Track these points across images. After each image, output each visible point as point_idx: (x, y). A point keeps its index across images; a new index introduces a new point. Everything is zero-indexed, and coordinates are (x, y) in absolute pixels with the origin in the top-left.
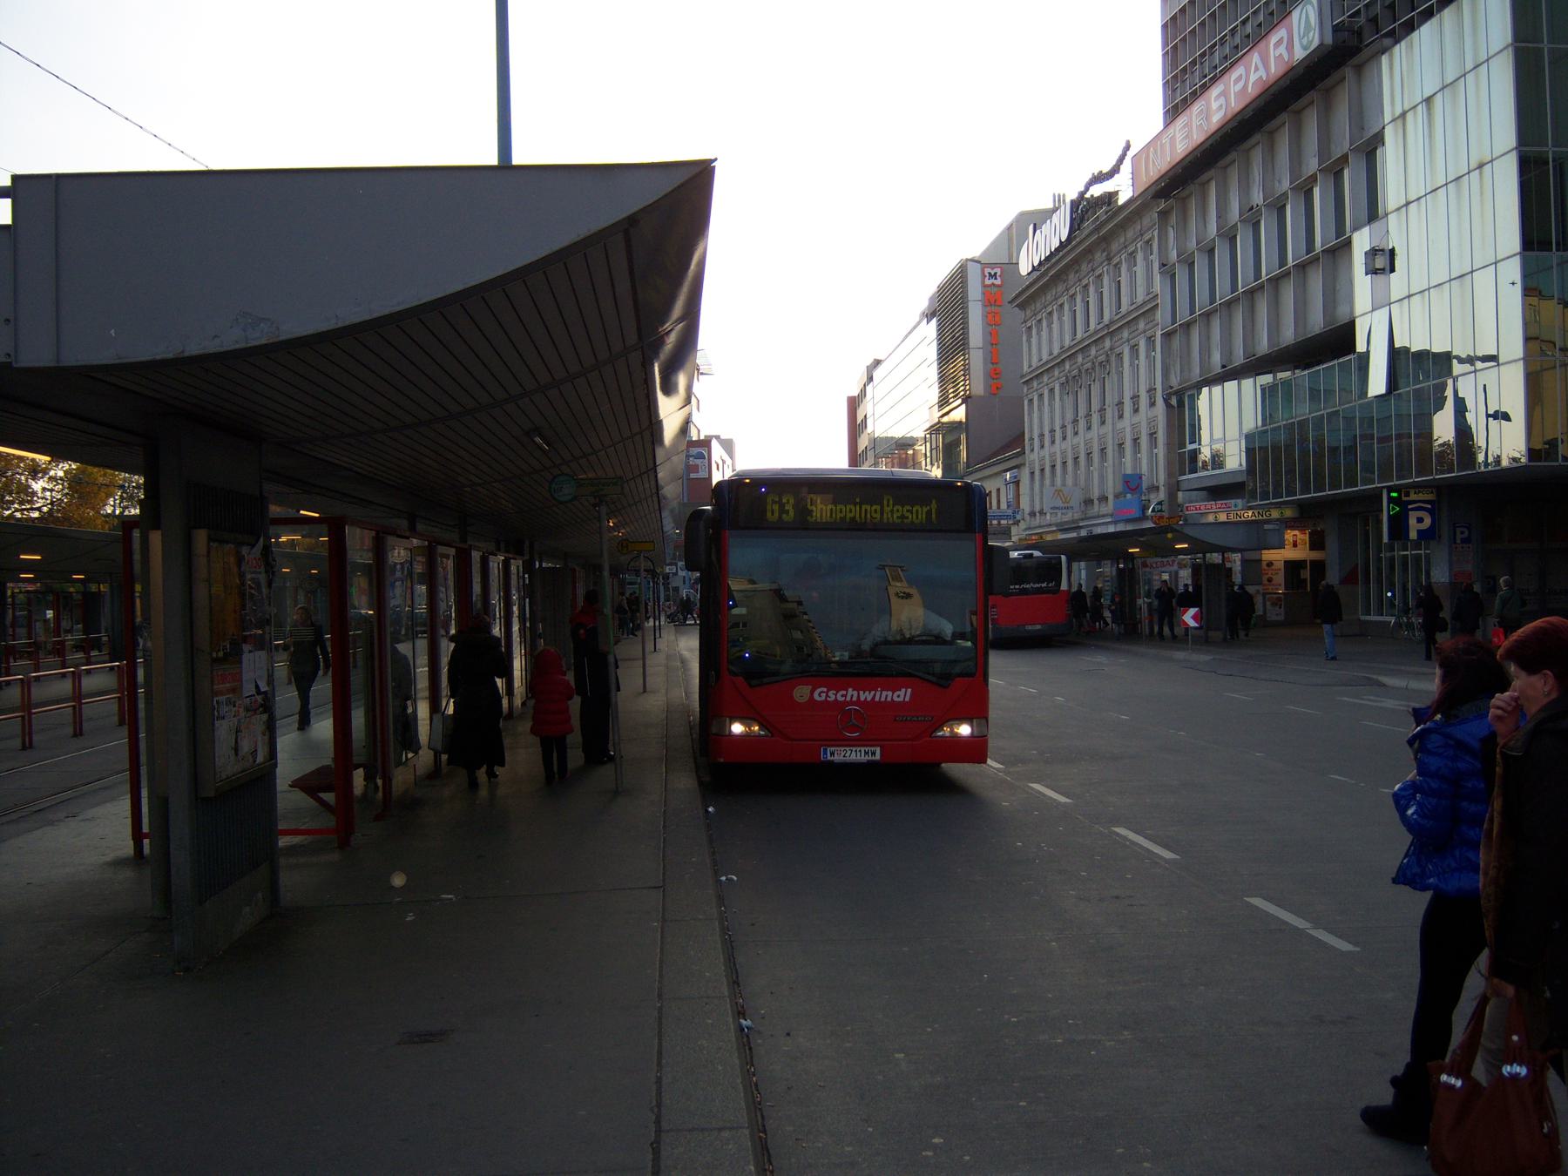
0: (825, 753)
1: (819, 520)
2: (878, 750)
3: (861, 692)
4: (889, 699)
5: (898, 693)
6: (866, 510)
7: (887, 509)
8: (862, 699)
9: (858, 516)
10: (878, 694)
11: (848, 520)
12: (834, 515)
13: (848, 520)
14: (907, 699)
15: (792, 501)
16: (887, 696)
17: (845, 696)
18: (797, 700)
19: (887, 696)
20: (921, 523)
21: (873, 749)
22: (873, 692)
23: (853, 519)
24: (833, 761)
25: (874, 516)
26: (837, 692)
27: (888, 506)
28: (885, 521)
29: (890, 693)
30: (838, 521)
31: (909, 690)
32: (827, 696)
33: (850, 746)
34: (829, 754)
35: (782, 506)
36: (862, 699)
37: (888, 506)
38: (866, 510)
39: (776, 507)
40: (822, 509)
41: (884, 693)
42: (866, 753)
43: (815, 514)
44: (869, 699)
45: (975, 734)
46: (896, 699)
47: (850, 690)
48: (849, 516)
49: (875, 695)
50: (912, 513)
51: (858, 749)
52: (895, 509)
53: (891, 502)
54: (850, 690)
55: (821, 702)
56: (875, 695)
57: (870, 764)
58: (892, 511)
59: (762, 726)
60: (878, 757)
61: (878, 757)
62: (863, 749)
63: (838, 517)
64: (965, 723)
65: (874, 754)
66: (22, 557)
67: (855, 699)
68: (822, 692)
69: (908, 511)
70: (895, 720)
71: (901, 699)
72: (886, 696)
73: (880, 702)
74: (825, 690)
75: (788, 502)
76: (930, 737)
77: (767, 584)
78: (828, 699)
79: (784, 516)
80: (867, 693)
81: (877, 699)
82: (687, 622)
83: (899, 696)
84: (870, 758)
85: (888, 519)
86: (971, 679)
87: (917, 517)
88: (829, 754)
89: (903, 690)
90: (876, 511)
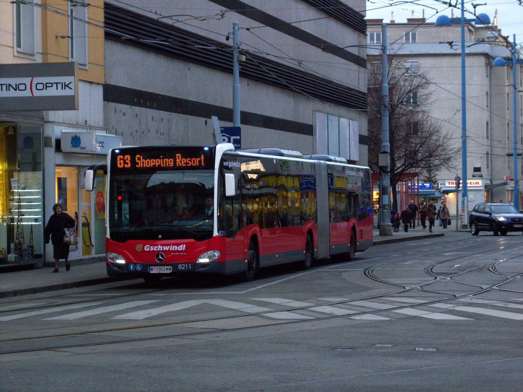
6: (166, 161)
14: (184, 249)
15: (129, 159)
22: (169, 247)
27: (179, 158)
30: (152, 166)
31: (184, 245)
32: (150, 249)
37: (179, 158)
38: (166, 161)
39: (122, 162)
40: (143, 162)
43: (139, 164)
44: (167, 249)
46: (179, 249)
53: (180, 157)
71: (181, 249)
74: (149, 246)
75: (127, 159)
80: (166, 247)
90: (171, 161)
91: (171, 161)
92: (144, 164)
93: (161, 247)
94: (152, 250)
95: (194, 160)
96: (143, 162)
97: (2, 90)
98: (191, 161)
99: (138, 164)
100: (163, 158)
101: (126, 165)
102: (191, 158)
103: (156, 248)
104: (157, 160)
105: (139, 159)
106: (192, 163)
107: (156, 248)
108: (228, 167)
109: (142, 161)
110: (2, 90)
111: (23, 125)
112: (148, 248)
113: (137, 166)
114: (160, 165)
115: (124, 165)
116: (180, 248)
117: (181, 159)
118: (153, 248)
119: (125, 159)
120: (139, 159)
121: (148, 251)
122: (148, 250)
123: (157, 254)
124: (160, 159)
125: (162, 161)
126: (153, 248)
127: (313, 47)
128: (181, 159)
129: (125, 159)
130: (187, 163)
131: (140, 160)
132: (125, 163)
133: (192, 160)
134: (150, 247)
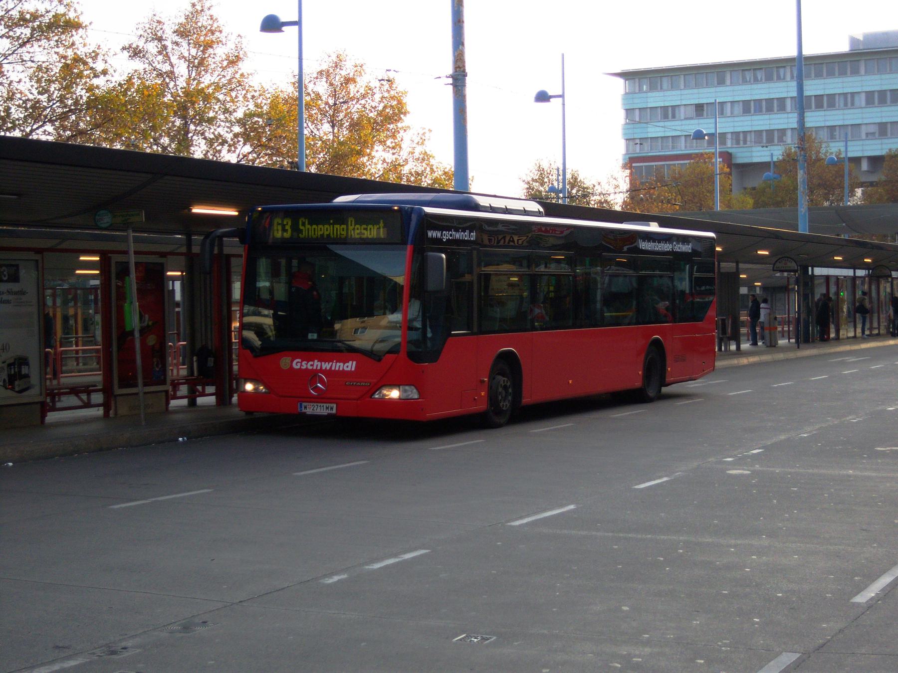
0: (301, 407)
1: (353, 237)
2: (335, 406)
3: (323, 363)
4: (341, 369)
5: (346, 364)
6: (337, 229)
7: (351, 228)
8: (324, 368)
9: (331, 234)
10: (334, 364)
11: (325, 236)
12: (316, 233)
13: (325, 236)
14: (353, 369)
15: (290, 223)
16: (317, 365)
17: (312, 365)
18: (282, 367)
19: (317, 365)
20: (317, 237)
21: (331, 405)
22: (331, 363)
23: (329, 235)
24: (305, 413)
25: (342, 233)
26: (308, 362)
27: (351, 225)
28: (310, 237)
29: (342, 364)
30: (319, 237)
31: (354, 363)
32: (301, 365)
33: (317, 402)
34: (303, 408)
35: (283, 226)
36: (324, 368)
37: (351, 225)
38: (337, 229)
39: (280, 227)
40: (308, 229)
41: (338, 364)
42: (327, 408)
43: (304, 233)
44: (328, 368)
45: (401, 397)
46: (346, 369)
47: (316, 361)
48: (326, 233)
49: (332, 365)
50: (340, 234)
51: (322, 405)
52: (356, 227)
53: (353, 223)
54: (316, 361)
55: (297, 369)
56: (332, 365)
57: (330, 415)
58: (354, 229)
59: (266, 387)
60: (334, 411)
61: (334, 411)
62: (325, 405)
63: (319, 234)
64: (395, 388)
65: (332, 409)
66: (759, 252)
67: (319, 368)
68: (297, 362)
69: (364, 229)
70: (345, 384)
71: (349, 369)
72: (339, 366)
73: (335, 371)
74: (300, 360)
75: (287, 224)
76: (371, 398)
77: (261, 286)
78: (302, 367)
79: (300, 235)
80: (327, 363)
81: (333, 368)
82: (858, 315)
83: (347, 367)
84: (330, 412)
85: (351, 235)
86: (396, 355)
87: (315, 234)
88: (303, 408)
89: (351, 362)
90: (343, 229)
91: (343, 229)
92: (310, 232)
93: (319, 363)
94: (304, 367)
95: (371, 229)
96: (308, 229)
97: (563, 55)
98: (366, 229)
99: (301, 231)
100: (333, 224)
101: (285, 234)
102: (367, 225)
103: (311, 365)
104: (326, 226)
105: (304, 224)
106: (369, 234)
107: (311, 365)
108: (442, 240)
109: (307, 228)
110: (563, 55)
111: (739, 155)
112: (299, 364)
113: (300, 235)
114: (330, 233)
115: (282, 234)
116: (347, 367)
117: (355, 225)
118: (307, 364)
119: (285, 223)
120: (304, 224)
121: (297, 370)
122: (298, 367)
123: (313, 375)
124: (330, 224)
125: (332, 228)
126: (307, 364)
127: (467, 70)
128: (355, 225)
129: (285, 223)
130: (360, 233)
131: (305, 227)
132: (284, 230)
133: (369, 229)
134: (301, 362)
